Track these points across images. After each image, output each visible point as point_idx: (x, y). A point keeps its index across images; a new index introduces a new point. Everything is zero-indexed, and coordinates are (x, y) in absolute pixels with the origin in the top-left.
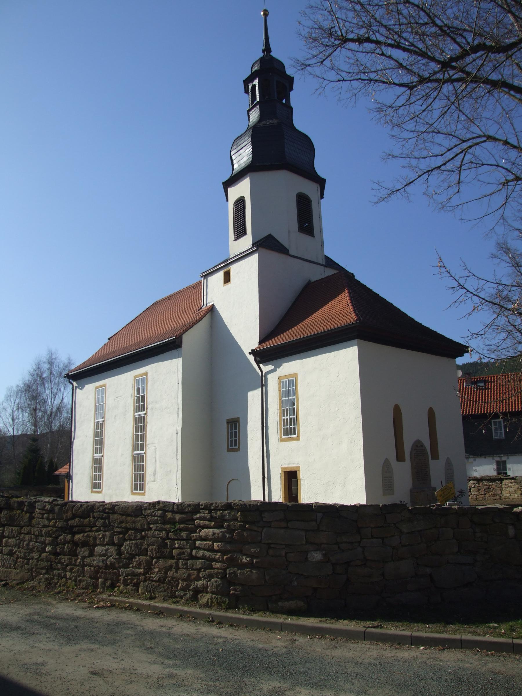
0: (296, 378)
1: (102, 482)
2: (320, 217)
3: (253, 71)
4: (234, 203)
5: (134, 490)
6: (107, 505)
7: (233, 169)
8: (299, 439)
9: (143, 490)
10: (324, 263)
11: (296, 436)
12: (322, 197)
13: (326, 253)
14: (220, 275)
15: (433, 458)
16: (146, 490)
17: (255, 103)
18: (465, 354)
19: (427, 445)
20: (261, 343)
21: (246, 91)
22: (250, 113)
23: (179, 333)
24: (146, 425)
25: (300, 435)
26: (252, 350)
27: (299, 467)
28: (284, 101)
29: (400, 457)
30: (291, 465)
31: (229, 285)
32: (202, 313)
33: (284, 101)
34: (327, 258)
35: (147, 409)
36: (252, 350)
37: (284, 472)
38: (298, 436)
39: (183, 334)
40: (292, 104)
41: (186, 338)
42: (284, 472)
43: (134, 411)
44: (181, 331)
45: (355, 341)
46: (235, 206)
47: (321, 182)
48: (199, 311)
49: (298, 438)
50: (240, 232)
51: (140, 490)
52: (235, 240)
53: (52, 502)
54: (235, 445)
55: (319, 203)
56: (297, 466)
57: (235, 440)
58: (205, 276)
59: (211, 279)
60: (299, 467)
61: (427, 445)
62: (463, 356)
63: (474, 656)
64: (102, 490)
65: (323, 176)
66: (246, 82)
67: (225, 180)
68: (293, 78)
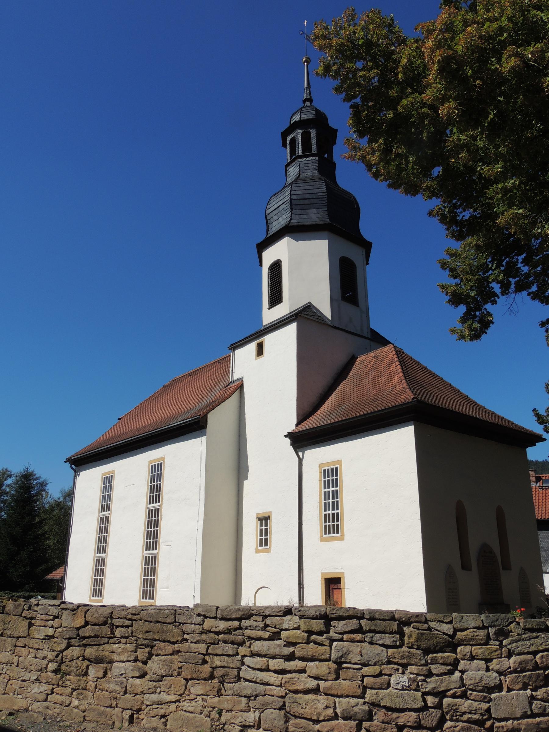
0: (341, 466)
1: (104, 588)
2: (365, 285)
3: (292, 122)
4: (269, 267)
5: (143, 598)
6: (131, 610)
7: (268, 230)
8: (343, 539)
9: (153, 599)
10: (369, 337)
11: (339, 535)
12: (367, 264)
13: (372, 326)
14: (252, 347)
15: (504, 568)
16: (157, 599)
17: (294, 157)
18: (537, 444)
19: (497, 550)
20: (298, 424)
21: (284, 145)
22: (288, 169)
23: (204, 411)
24: (161, 520)
25: (345, 534)
26: (288, 433)
27: (343, 573)
28: (326, 156)
29: (466, 566)
30: (333, 571)
31: (262, 359)
32: (230, 391)
33: (326, 156)
34: (372, 331)
35: (162, 500)
36: (288, 433)
37: (325, 579)
38: (343, 535)
39: (208, 413)
40: (335, 160)
41: (213, 419)
42: (325, 579)
43: (147, 502)
44: (206, 410)
45: (412, 422)
46: (270, 273)
47: (367, 246)
48: (227, 388)
49: (342, 538)
50: (276, 267)
51: (149, 599)
52: (269, 309)
53: (59, 606)
54: (266, 544)
55: (364, 270)
56: (341, 571)
57: (265, 539)
58: (235, 347)
59: (240, 353)
60: (343, 573)
61: (497, 550)
62: (535, 445)
63: (381, 659)
64: (103, 599)
65: (368, 239)
66: (285, 135)
67: (259, 242)
68: (336, 130)
